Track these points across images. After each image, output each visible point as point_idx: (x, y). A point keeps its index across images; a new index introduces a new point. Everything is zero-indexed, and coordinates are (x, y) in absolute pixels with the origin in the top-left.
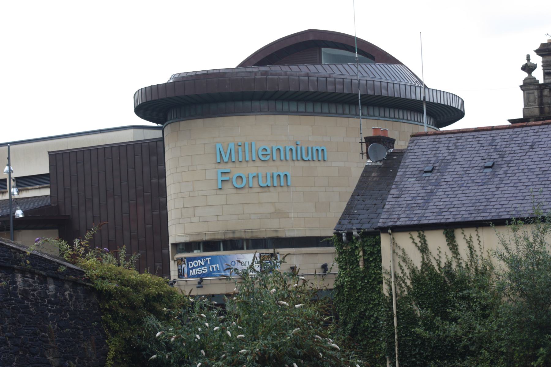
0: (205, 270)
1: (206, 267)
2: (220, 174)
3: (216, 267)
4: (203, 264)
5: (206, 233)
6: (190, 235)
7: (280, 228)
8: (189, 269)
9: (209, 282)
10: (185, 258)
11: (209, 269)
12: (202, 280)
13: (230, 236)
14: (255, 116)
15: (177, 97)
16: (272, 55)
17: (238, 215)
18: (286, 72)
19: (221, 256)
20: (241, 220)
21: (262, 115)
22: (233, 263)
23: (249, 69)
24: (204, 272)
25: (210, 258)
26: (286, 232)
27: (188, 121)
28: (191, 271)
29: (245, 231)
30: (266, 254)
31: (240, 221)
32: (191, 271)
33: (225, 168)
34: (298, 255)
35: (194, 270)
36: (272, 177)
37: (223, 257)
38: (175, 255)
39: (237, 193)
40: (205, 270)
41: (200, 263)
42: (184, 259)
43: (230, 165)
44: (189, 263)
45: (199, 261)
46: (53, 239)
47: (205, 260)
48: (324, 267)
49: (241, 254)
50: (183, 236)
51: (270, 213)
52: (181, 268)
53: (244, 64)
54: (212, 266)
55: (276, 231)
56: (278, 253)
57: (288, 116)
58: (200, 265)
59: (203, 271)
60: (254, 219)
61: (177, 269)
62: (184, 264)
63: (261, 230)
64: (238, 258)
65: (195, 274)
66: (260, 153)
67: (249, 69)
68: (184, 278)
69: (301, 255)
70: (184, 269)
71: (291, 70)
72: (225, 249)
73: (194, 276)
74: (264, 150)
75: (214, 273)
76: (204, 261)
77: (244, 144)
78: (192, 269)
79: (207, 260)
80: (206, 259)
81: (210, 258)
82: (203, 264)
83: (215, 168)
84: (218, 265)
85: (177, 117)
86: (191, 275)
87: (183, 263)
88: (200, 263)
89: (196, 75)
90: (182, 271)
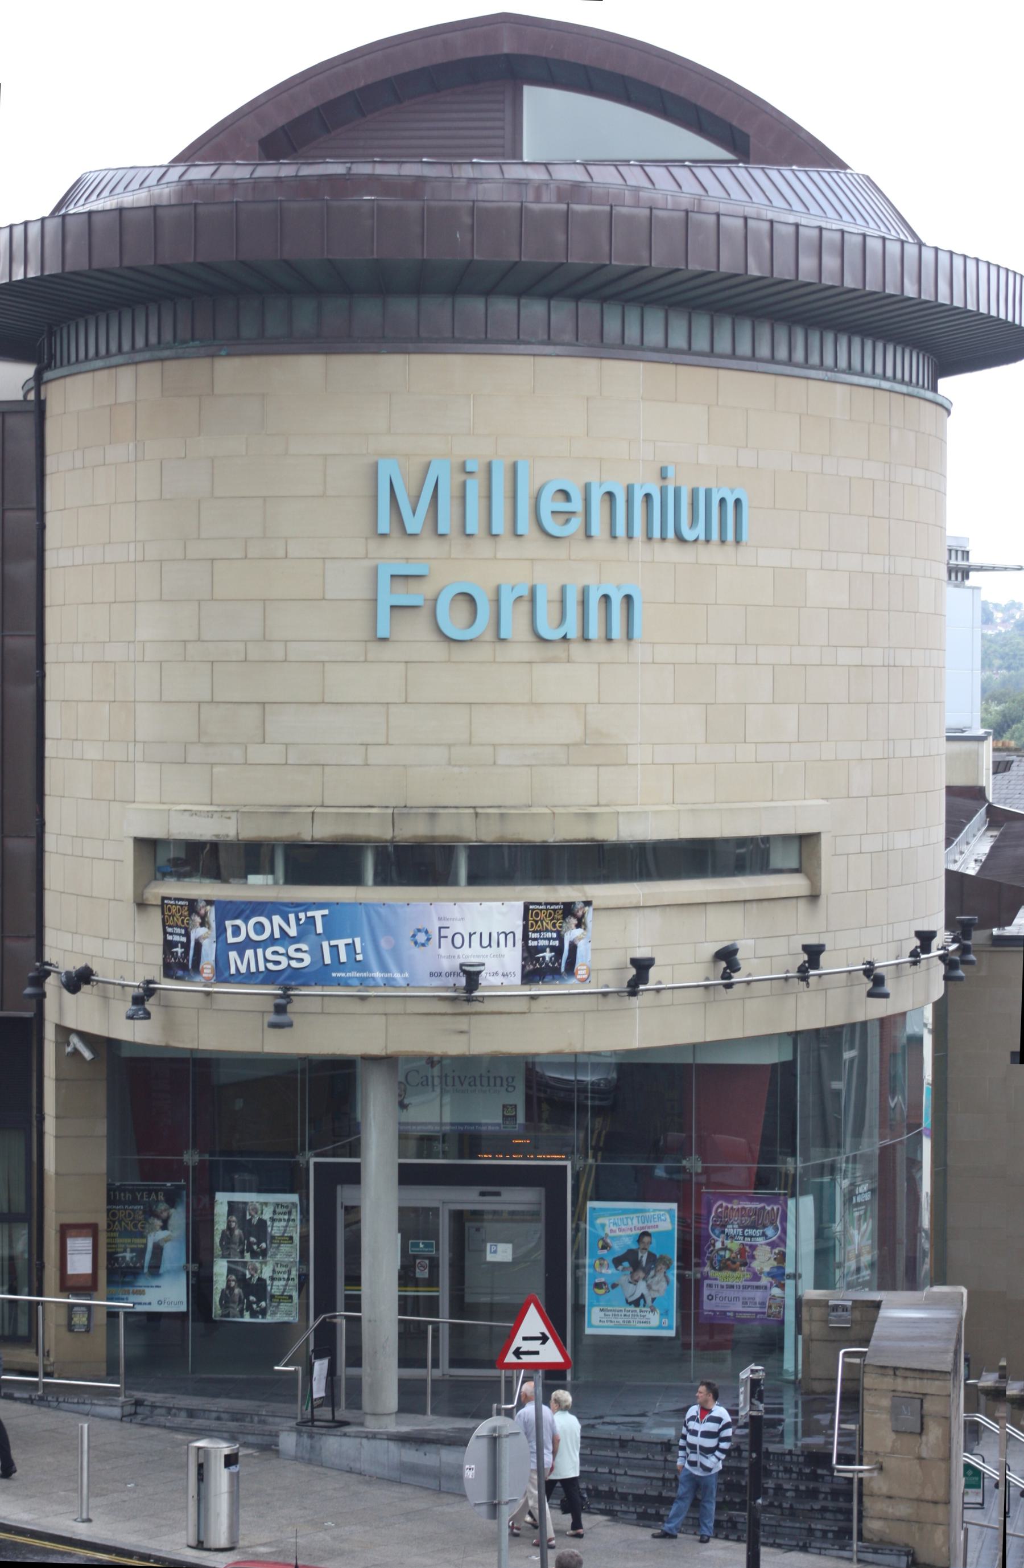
0: (299, 955)
1: (304, 947)
2: (384, 581)
3: (351, 947)
4: (293, 931)
5: (318, 810)
6: (242, 813)
7: (598, 805)
8: (223, 948)
9: (315, 1006)
10: (209, 902)
11: (317, 952)
12: (289, 996)
13: (414, 830)
14: (532, 358)
15: (202, 264)
16: (296, 123)
17: (450, 746)
18: (637, 189)
19: (373, 905)
20: (460, 766)
21: (558, 356)
22: (421, 938)
23: (228, 172)
24: (294, 964)
25: (326, 912)
26: (621, 818)
27: (255, 360)
28: (233, 955)
29: (477, 814)
30: (546, 904)
31: (456, 770)
32: (233, 955)
33: (407, 559)
34: (647, 911)
35: (249, 953)
36: (584, 603)
37: (383, 910)
38: (146, 886)
39: (449, 661)
40: (299, 955)
41: (281, 928)
42: (202, 904)
43: (428, 548)
44: (228, 924)
45: (277, 919)
46: (893, 1098)
47: (302, 915)
48: (727, 957)
49: (455, 901)
50: (210, 814)
51: (568, 745)
52: (184, 939)
53: (189, 156)
54: (333, 943)
55: (590, 816)
56: (588, 903)
57: (641, 365)
58: (277, 935)
59: (290, 958)
60: (510, 766)
61: (161, 942)
62: (203, 924)
63: (534, 810)
64: (440, 919)
65: (253, 969)
66: (547, 506)
67: (228, 172)
68: (198, 979)
69: (658, 909)
70: (198, 945)
71: (653, 183)
72: (383, 879)
73: (249, 978)
74: (560, 496)
75: (338, 971)
76: (298, 919)
77: (489, 466)
78: (240, 949)
79: (313, 917)
80: (309, 914)
81: (326, 912)
82: (293, 931)
83: (366, 557)
84: (358, 941)
85: (159, 342)
86: (233, 971)
87: (198, 920)
88: (281, 928)
89: (296, 176)
90: (186, 953)
